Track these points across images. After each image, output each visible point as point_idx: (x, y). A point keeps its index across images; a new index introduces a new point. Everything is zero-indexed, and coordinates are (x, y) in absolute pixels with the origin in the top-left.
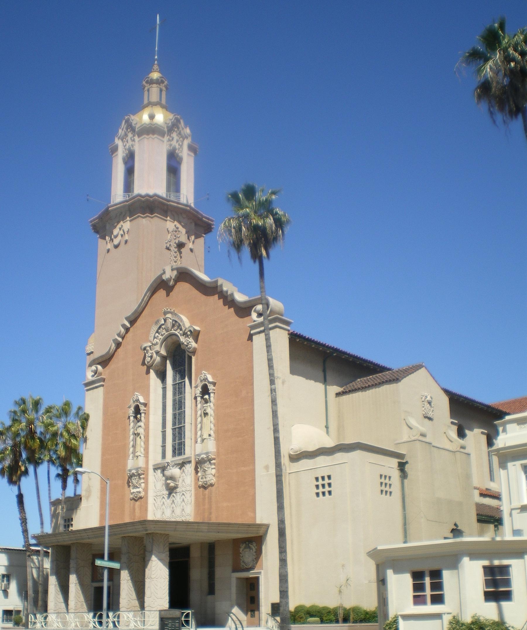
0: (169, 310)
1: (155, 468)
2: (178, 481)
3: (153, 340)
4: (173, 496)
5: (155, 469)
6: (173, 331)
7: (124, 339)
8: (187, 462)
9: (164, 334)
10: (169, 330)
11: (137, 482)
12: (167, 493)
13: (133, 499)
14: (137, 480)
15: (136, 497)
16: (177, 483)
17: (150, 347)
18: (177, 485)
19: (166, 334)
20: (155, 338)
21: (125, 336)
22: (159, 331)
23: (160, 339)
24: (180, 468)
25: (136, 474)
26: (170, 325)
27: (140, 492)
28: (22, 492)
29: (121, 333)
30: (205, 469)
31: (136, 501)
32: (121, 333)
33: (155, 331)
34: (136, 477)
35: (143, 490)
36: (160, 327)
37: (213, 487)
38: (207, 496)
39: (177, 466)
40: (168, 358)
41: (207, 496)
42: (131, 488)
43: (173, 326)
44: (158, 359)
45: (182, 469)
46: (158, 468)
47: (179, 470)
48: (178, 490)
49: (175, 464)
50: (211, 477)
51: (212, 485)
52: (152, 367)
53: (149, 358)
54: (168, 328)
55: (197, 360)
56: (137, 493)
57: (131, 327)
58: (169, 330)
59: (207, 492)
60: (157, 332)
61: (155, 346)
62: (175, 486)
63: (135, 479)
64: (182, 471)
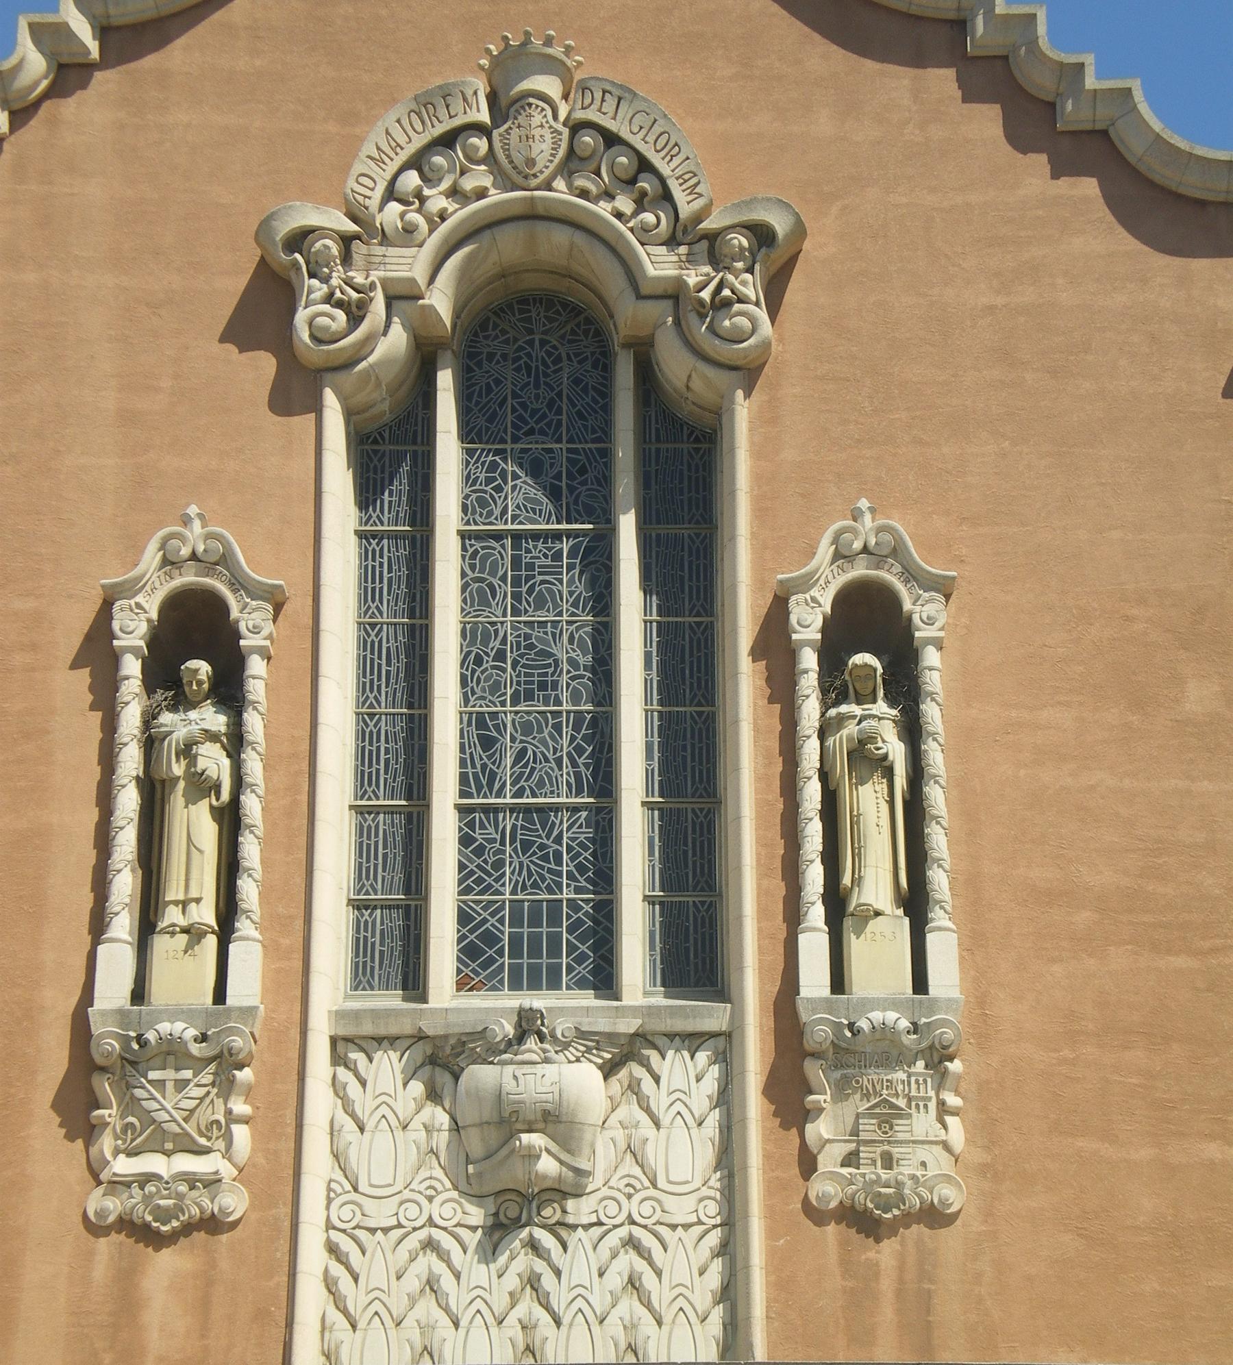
0: (557, 51)
1: (342, 1032)
2: (586, 1151)
3: (381, 210)
4: (533, 1246)
5: (348, 1040)
6: (561, 191)
7: (24, 123)
8: (671, 1036)
9: (481, 194)
10: (534, 182)
11: (191, 1104)
12: (476, 1215)
13: (128, 1226)
14: (200, 1092)
15: (163, 1215)
16: (584, 1165)
17: (346, 240)
18: (578, 1172)
19: (496, 196)
20: (391, 194)
21: (37, 104)
22: (438, 160)
23: (443, 216)
24: (609, 1070)
25: (195, 1049)
26: (546, 146)
27: (212, 1183)
28: (88, 939)
29: (24, 80)
30: (893, 1106)
31: (156, 1240)
32: (24, 80)
33: (403, 156)
34: (187, 1074)
35: (240, 1171)
36: (447, 141)
37: (943, 1231)
38: (887, 1285)
39: (589, 1050)
40: (446, 357)
41: (887, 1285)
42: (107, 1143)
43: (572, 162)
44: (396, 341)
45: (623, 1073)
46: (379, 1040)
47: (599, 1075)
48: (580, 1210)
49: (582, 1034)
50: (939, 1163)
51: (950, 1219)
52: (341, 377)
53: (341, 316)
54: (531, 162)
55: (768, 419)
56: (183, 1188)
57: (106, 62)
58: (534, 182)
59: (886, 1253)
60: (416, 162)
61: (392, 251)
62: (560, 1178)
63: (181, 1085)
64: (616, 1085)
